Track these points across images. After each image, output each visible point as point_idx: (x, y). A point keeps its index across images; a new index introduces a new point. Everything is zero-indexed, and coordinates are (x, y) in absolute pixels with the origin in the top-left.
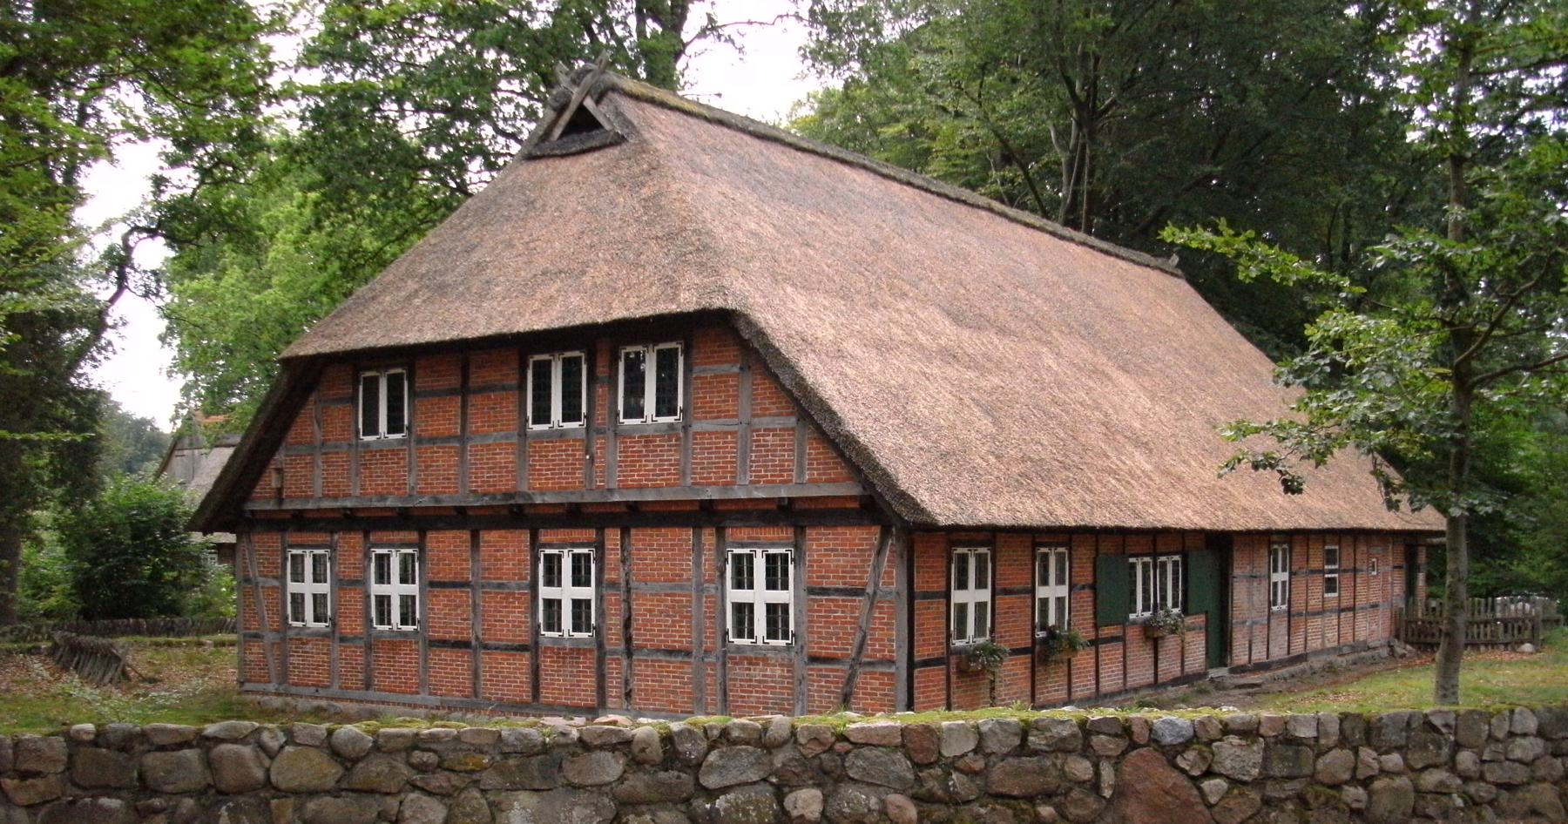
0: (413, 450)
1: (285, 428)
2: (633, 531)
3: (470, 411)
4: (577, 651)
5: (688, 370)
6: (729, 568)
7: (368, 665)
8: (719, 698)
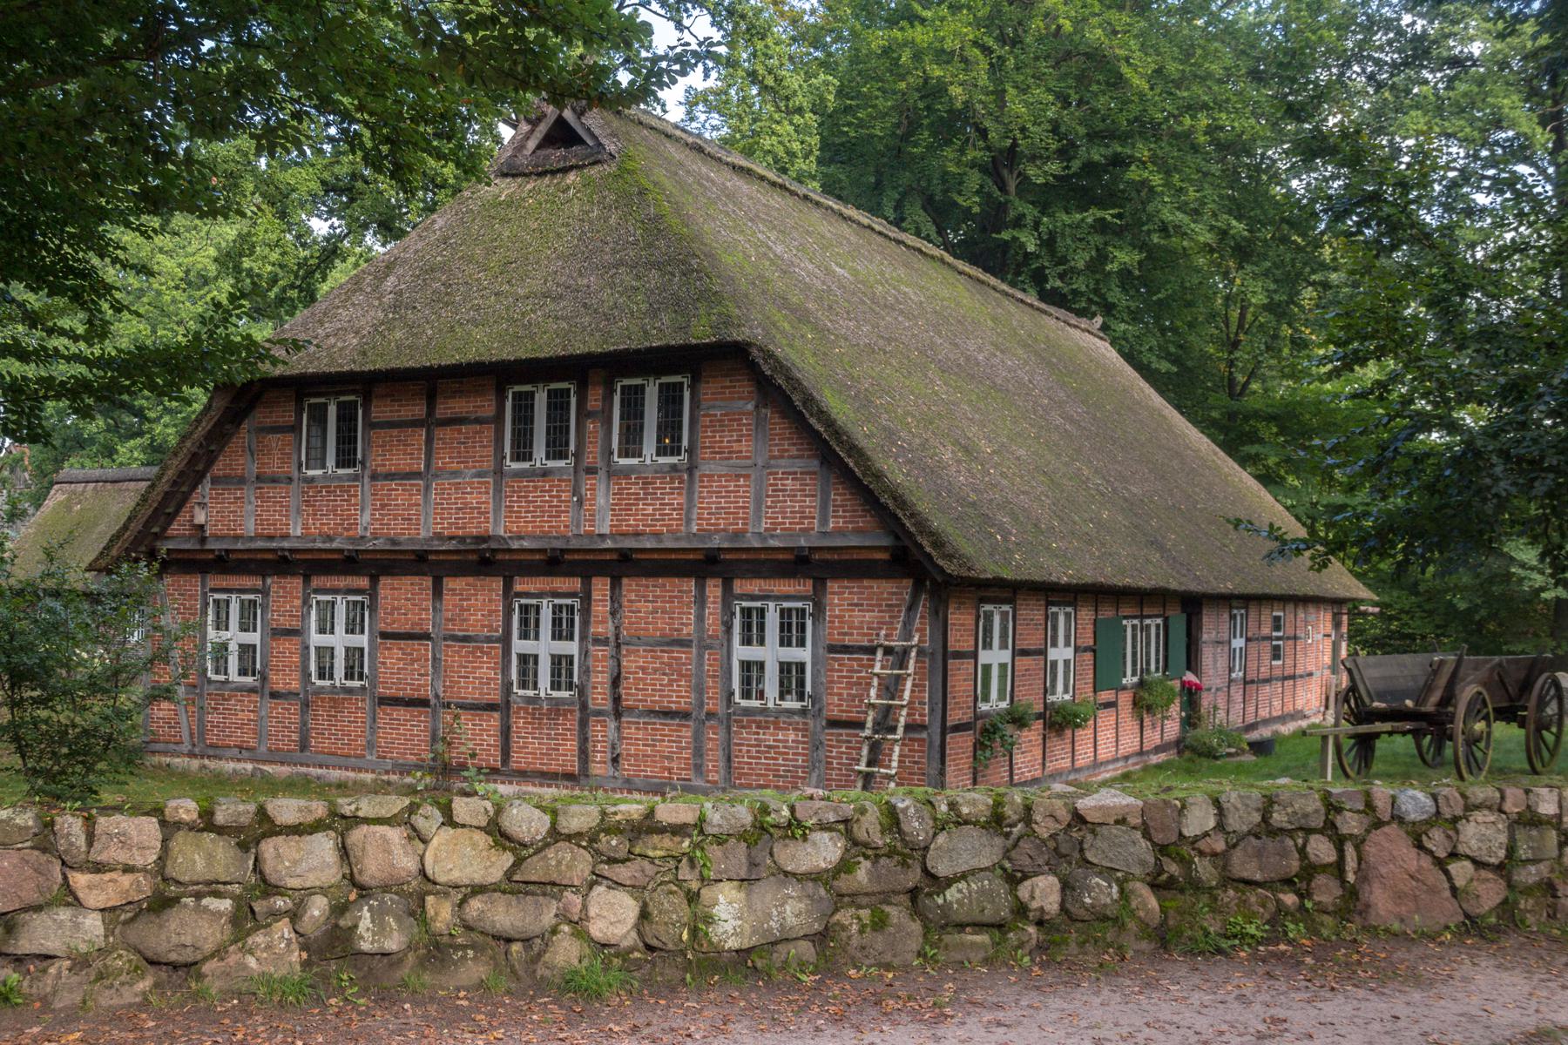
0: (366, 487)
1: (211, 460)
2: (625, 581)
3: (437, 444)
4: (557, 707)
5: (695, 405)
6: (737, 622)
7: (304, 724)
8: (722, 764)
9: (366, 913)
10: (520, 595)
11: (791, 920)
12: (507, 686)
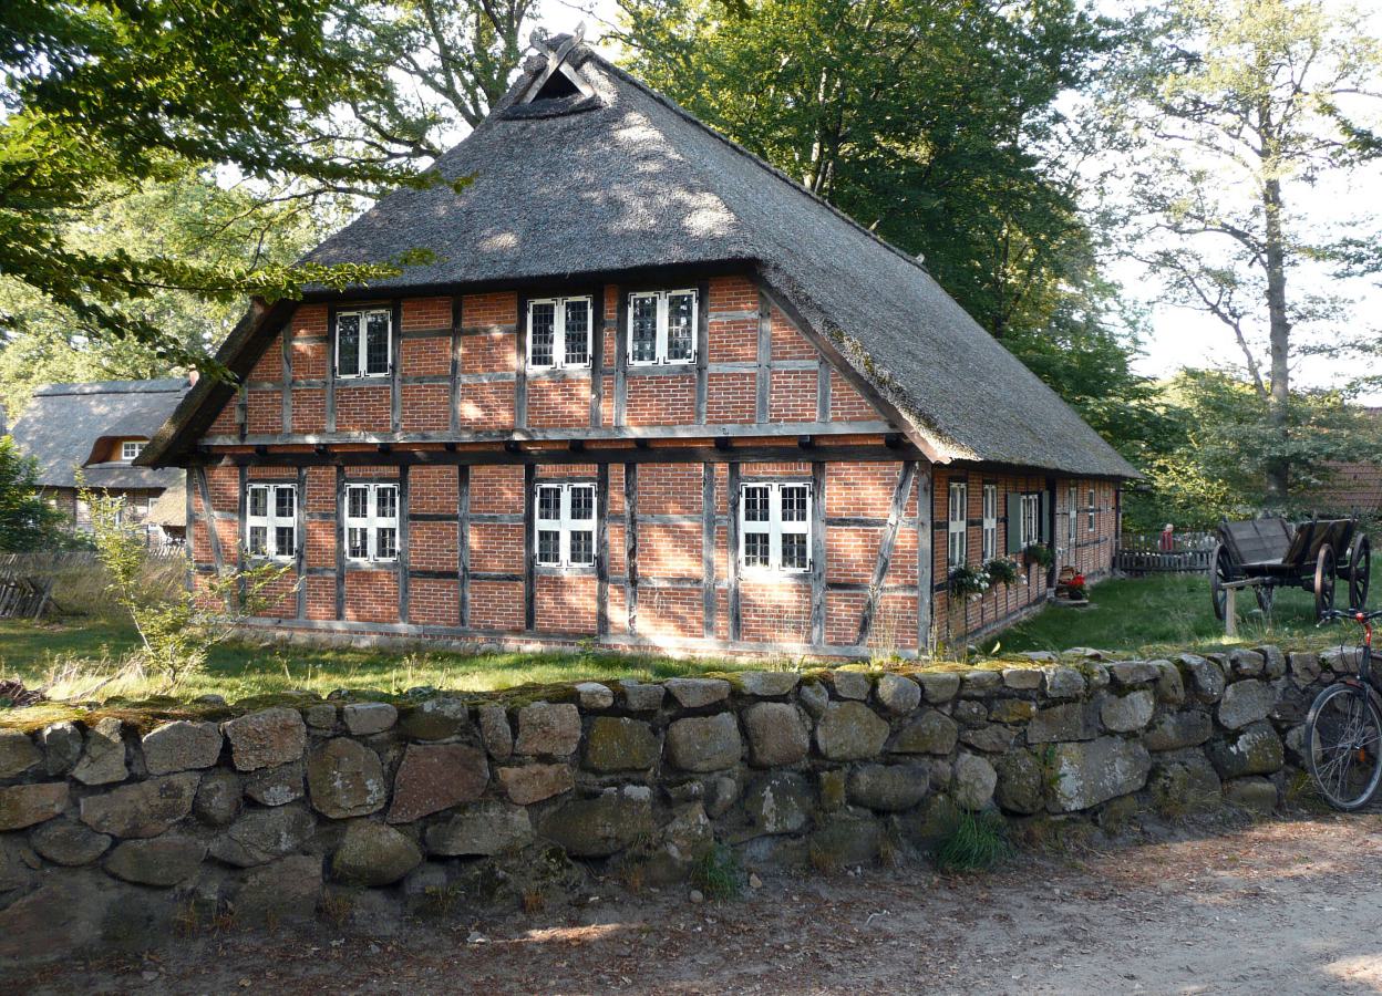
2: (639, 467)
9: (768, 794)
10: (747, 479)
11: (1121, 778)
12: (531, 562)
